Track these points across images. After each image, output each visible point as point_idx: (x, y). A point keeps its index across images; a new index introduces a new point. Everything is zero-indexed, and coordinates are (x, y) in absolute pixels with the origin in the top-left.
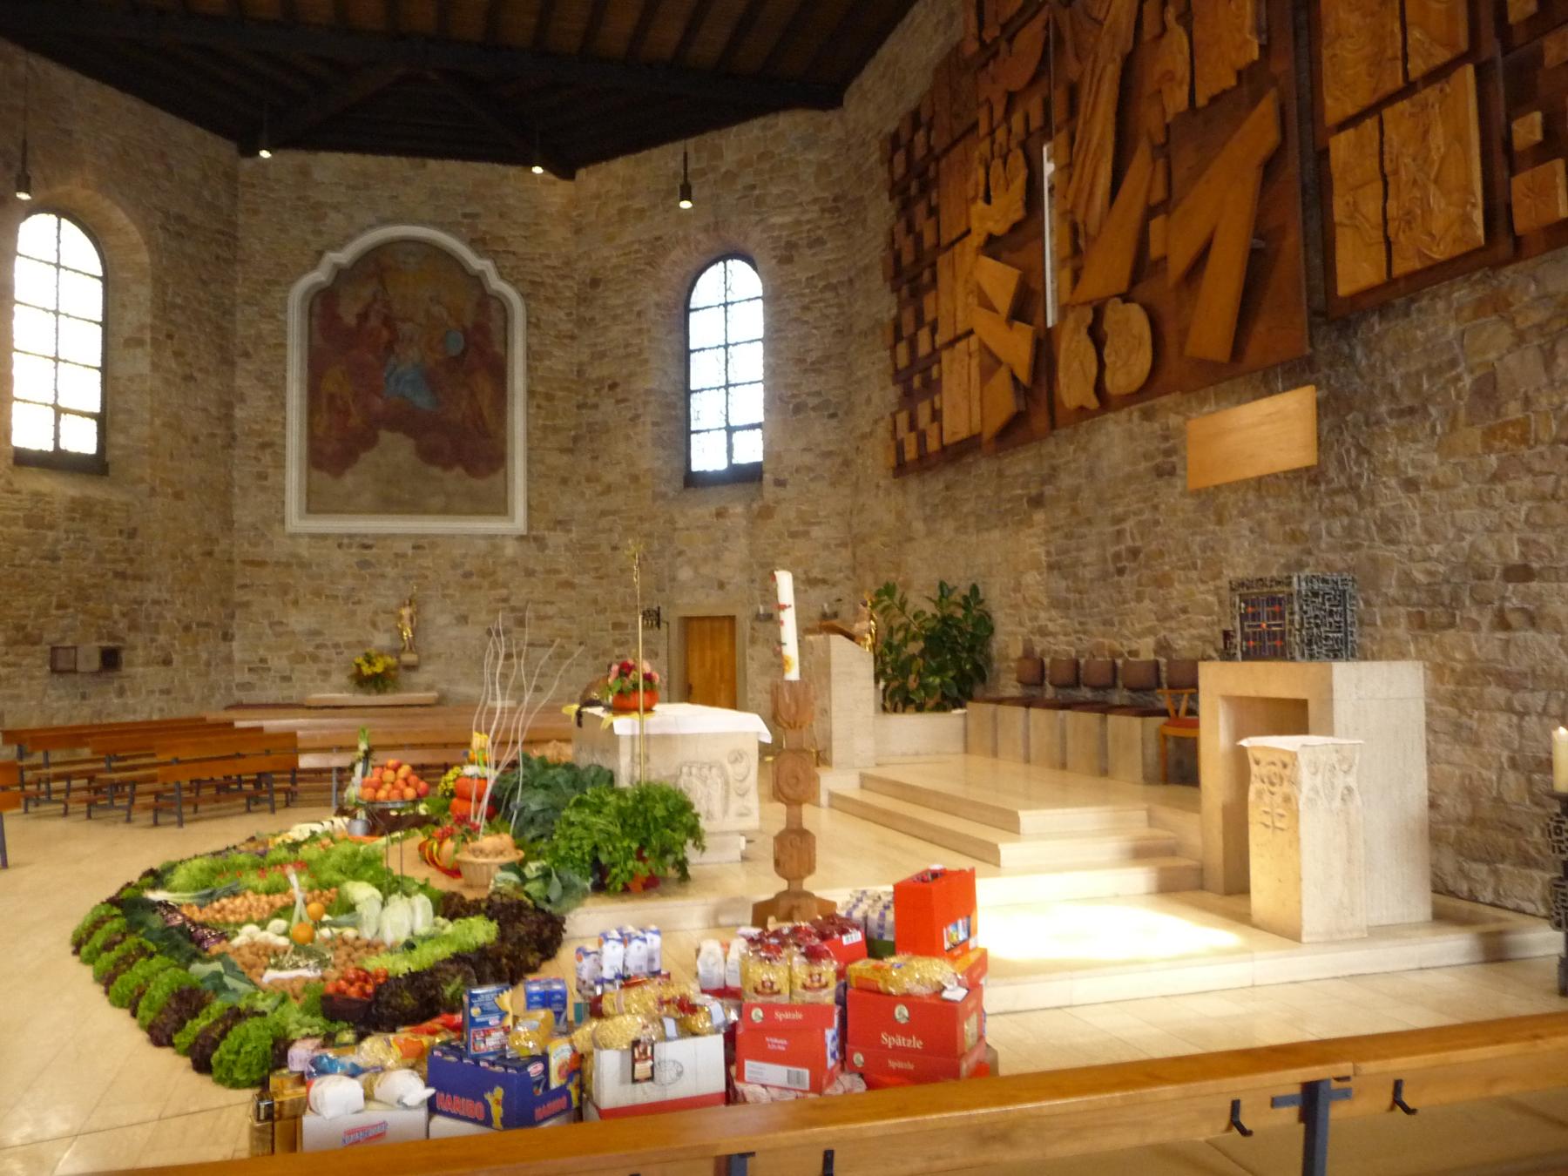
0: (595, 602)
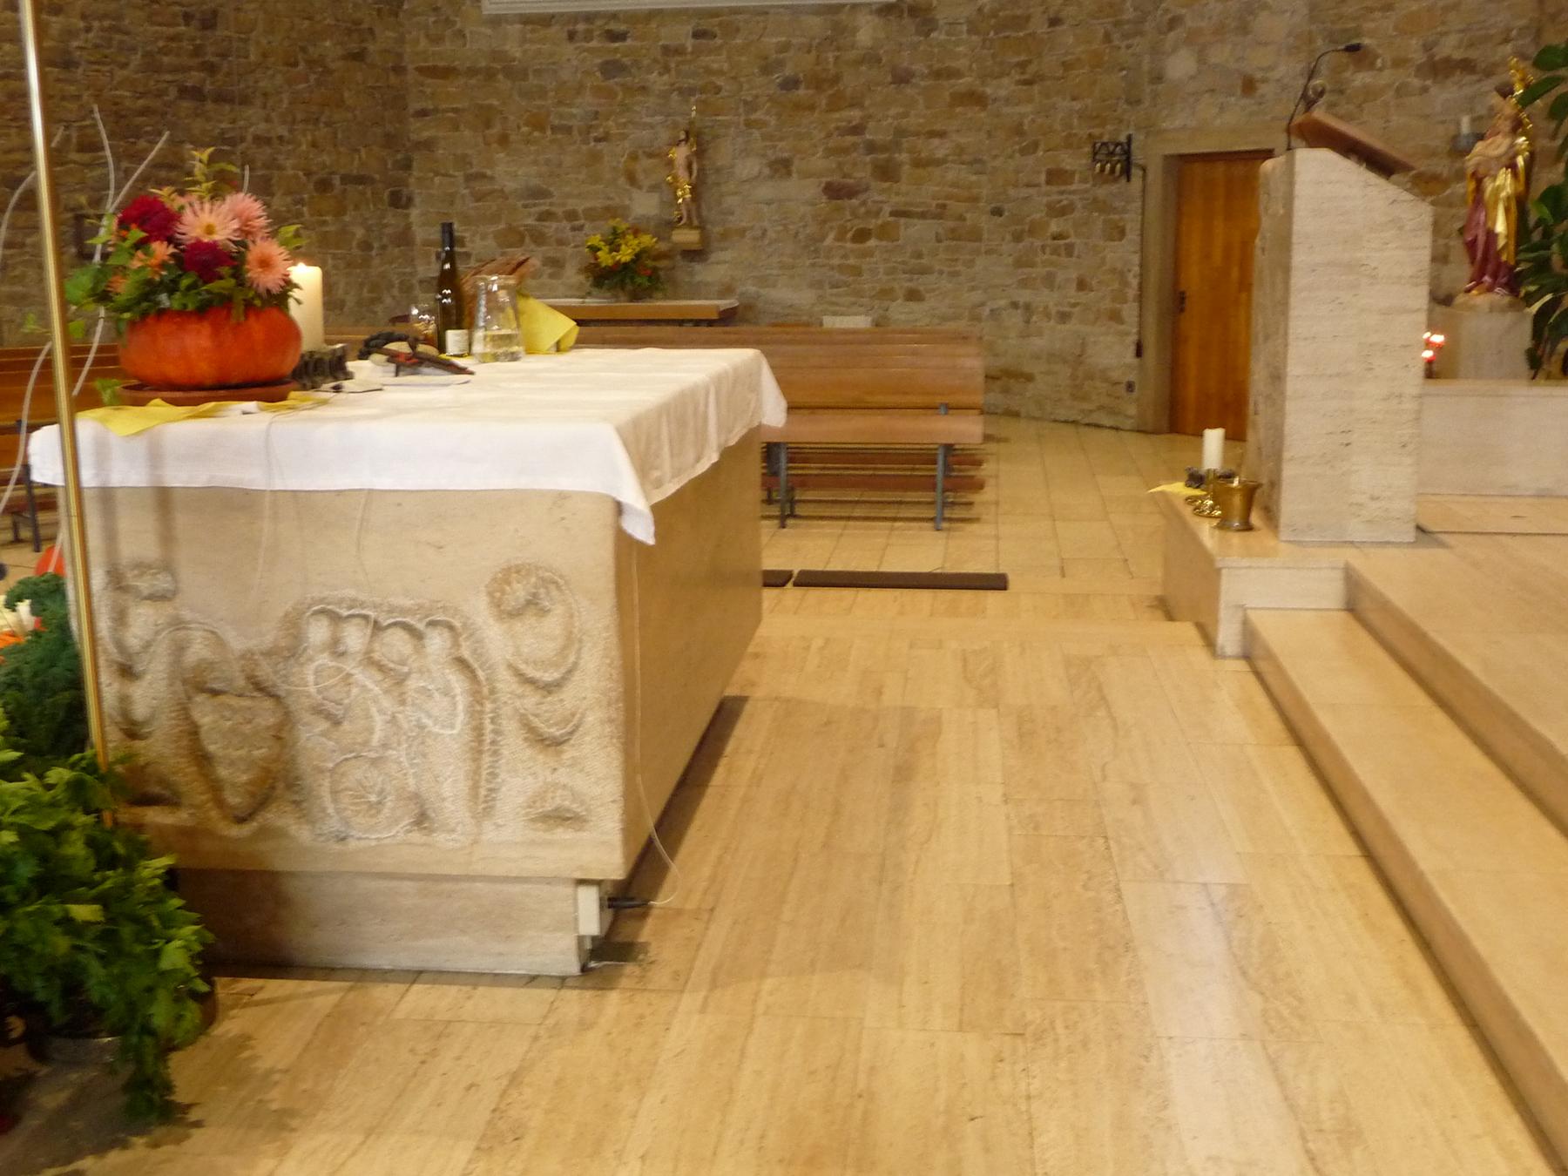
0: (1018, 131)
